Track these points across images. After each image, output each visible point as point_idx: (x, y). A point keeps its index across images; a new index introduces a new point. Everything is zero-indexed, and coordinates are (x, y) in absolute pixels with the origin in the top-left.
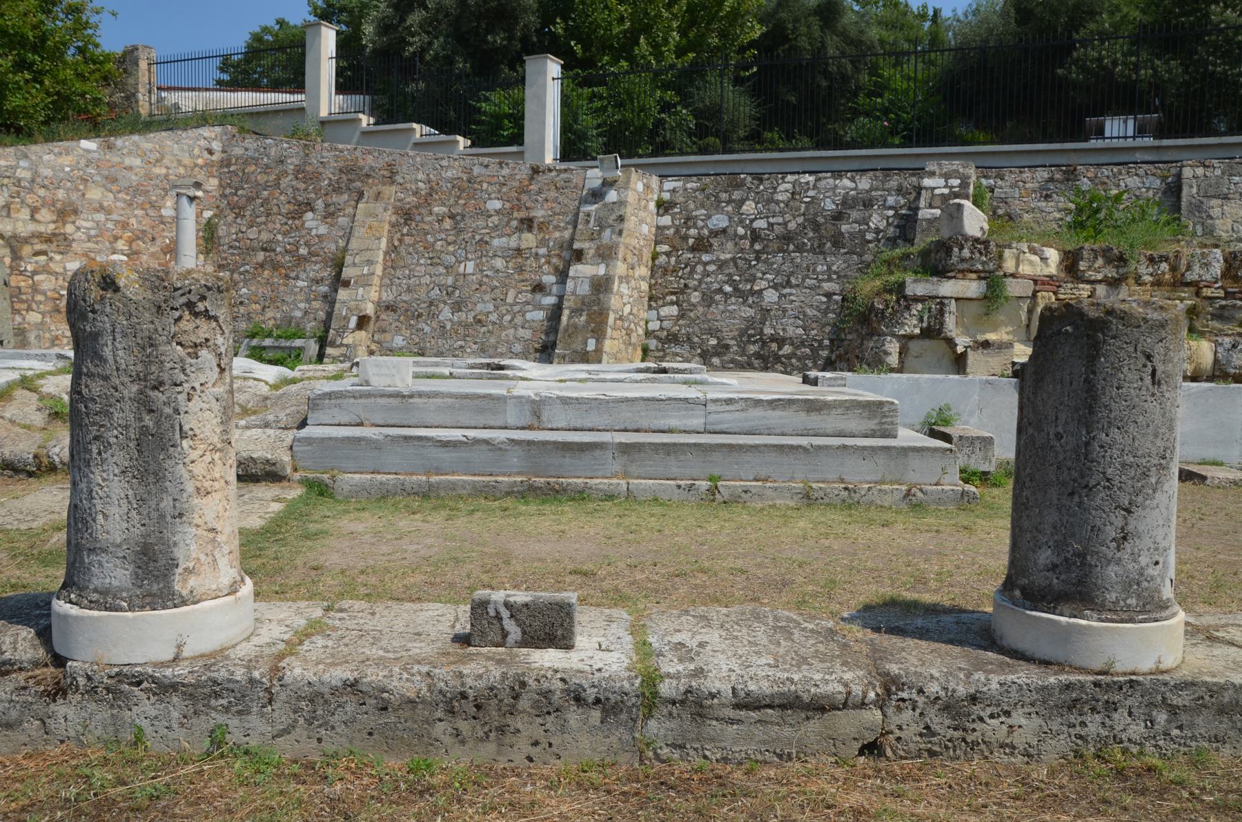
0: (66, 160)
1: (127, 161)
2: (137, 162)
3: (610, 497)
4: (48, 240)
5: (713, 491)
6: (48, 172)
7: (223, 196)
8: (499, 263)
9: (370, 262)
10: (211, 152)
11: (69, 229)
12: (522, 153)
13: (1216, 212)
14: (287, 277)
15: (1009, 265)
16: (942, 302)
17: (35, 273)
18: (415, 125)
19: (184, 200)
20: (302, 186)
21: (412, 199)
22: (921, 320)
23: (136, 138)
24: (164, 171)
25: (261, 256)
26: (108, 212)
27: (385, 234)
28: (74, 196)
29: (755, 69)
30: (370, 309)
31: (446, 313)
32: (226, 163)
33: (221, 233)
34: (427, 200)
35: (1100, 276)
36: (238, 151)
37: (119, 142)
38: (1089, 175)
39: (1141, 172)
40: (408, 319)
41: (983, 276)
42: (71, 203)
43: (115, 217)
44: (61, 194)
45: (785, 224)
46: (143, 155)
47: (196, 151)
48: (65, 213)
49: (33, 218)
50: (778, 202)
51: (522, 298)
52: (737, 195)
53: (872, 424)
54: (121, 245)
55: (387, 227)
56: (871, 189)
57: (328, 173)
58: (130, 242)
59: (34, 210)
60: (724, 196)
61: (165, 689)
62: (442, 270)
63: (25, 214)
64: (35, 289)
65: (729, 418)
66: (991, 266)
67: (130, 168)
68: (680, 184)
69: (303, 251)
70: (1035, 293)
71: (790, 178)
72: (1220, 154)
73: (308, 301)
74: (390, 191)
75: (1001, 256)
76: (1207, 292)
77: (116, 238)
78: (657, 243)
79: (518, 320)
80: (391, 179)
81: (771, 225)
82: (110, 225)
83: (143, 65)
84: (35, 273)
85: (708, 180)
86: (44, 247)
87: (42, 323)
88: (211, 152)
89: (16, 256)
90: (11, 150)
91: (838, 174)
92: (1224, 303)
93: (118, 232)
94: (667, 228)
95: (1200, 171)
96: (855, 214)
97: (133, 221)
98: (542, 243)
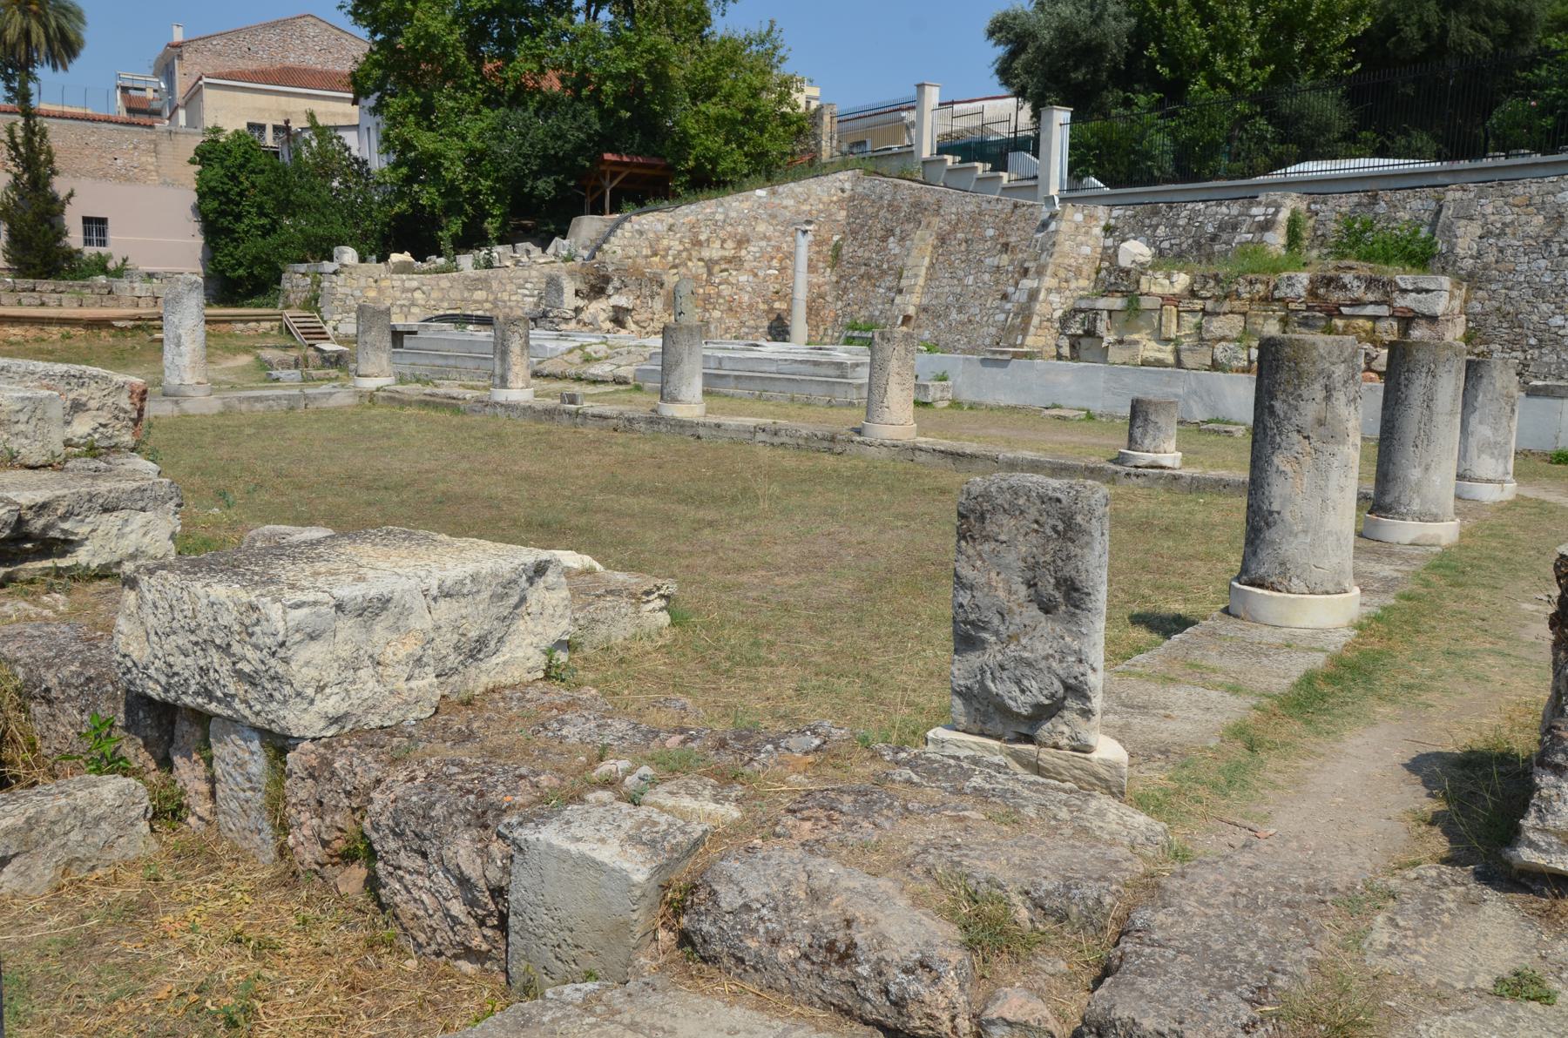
0: (746, 205)
1: (785, 202)
2: (790, 202)
3: (727, 396)
4: (730, 262)
5: (760, 396)
6: (734, 214)
7: (848, 224)
8: (986, 277)
9: (916, 276)
10: (843, 191)
11: (743, 253)
12: (1036, 186)
13: (1459, 232)
14: (875, 286)
15: (1144, 287)
16: (1096, 312)
17: (720, 284)
18: (976, 164)
19: (800, 233)
20: (890, 216)
21: (947, 228)
22: (1083, 324)
23: (792, 185)
24: (808, 208)
25: (863, 269)
26: (769, 239)
27: (928, 253)
28: (748, 230)
29: (1359, 65)
30: (911, 311)
31: (954, 315)
32: (852, 198)
33: (844, 252)
34: (955, 228)
35: (1209, 295)
36: (860, 189)
37: (780, 189)
38: (1387, 199)
39: (1424, 194)
40: (934, 318)
41: (1125, 294)
42: (746, 235)
43: (773, 243)
44: (740, 229)
45: (1180, 244)
46: (795, 197)
47: (833, 191)
48: (742, 242)
49: (722, 247)
50: (1178, 227)
51: (996, 304)
52: (1155, 221)
53: (838, 373)
54: (775, 263)
55: (930, 248)
56: (1239, 215)
57: (905, 208)
58: (781, 261)
59: (724, 241)
60: (1147, 221)
61: (502, 405)
62: (956, 282)
63: (717, 244)
64: (719, 295)
65: (785, 367)
66: (1131, 289)
67: (786, 207)
68: (1121, 212)
69: (885, 266)
70: (1162, 306)
71: (1190, 206)
72: (1476, 177)
73: (883, 304)
74: (936, 221)
75: (1138, 282)
76: (1292, 306)
77: (772, 258)
78: (1102, 260)
79: (991, 321)
80: (937, 213)
81: (1172, 245)
82: (769, 249)
83: (827, 119)
84: (720, 284)
85: (1139, 208)
86: (726, 266)
87: (721, 318)
88: (843, 191)
89: (710, 273)
90: (714, 201)
91: (1220, 202)
92: (1306, 314)
93: (774, 254)
94: (1109, 248)
95: (1459, 194)
96: (1225, 236)
97: (784, 245)
98: (1012, 262)
